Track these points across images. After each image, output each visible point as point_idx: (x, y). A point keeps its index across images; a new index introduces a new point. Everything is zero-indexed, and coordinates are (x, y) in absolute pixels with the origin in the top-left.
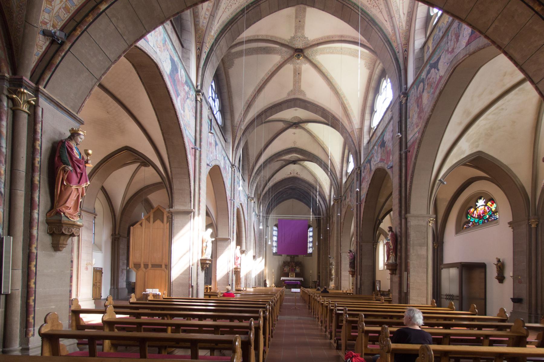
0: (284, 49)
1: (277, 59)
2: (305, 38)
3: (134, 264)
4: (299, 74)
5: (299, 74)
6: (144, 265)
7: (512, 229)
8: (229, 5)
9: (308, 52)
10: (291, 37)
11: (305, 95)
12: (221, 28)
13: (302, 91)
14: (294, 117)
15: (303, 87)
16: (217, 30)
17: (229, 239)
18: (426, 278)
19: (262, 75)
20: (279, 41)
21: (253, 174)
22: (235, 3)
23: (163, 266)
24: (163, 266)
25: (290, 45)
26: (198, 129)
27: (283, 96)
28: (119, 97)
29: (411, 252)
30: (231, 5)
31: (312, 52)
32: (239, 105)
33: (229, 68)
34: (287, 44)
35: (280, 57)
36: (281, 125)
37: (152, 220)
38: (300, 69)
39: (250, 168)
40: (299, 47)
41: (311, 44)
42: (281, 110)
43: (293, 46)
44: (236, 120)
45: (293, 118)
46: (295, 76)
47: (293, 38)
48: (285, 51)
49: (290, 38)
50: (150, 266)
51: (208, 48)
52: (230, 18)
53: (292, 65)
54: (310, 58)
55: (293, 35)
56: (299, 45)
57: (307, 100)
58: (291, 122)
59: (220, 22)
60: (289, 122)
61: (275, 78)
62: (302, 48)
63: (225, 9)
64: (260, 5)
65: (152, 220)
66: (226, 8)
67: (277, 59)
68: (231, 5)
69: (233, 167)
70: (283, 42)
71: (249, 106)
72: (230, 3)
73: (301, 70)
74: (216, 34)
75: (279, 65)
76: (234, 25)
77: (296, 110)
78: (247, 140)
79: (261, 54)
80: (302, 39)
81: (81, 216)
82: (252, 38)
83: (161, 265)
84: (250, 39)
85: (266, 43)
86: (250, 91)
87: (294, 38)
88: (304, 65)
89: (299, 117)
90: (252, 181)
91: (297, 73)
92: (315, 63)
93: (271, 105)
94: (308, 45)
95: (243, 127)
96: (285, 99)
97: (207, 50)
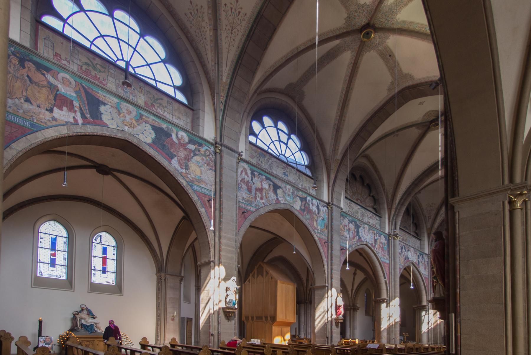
0: (348, 39)
1: (347, 57)
2: (363, 6)
3: (246, 317)
4: (390, 56)
5: (390, 56)
6: (251, 317)
7: (155, 134)
8: (232, 40)
9: (380, 20)
10: (345, 19)
11: (412, 77)
12: (232, 69)
13: (406, 74)
14: (427, 113)
15: (405, 70)
16: (229, 74)
17: (325, 286)
18: (461, 327)
19: (340, 86)
20: (331, 35)
21: (395, 205)
22: (238, 34)
23: (264, 318)
24: (264, 318)
25: (350, 29)
26: (218, 180)
27: (383, 95)
28: (143, 177)
29: (461, 274)
30: (234, 40)
31: (386, 15)
32: (327, 135)
33: (301, 101)
34: (345, 31)
35: (350, 52)
36: (415, 132)
37: (256, 276)
38: (387, 48)
39: (390, 200)
40: (363, 23)
41: (375, 8)
42: (389, 115)
43: (355, 28)
44: (328, 152)
45: (424, 116)
46: (387, 63)
47: (349, 19)
48: (352, 41)
49: (344, 21)
50: (255, 318)
51: (223, 97)
52: (238, 53)
53: (372, 51)
54: (389, 25)
55: (346, 16)
56: (361, 20)
57: (417, 82)
58: (425, 122)
59: (229, 63)
60: (424, 123)
61: (358, 82)
62: (367, 21)
63: (228, 48)
64: (262, 15)
65: (256, 276)
66: (229, 46)
67: (347, 57)
68: (234, 40)
69: (329, 206)
70: (338, 32)
71: (338, 130)
72: (232, 38)
73: (389, 49)
74: (229, 78)
75: (353, 62)
76: (243, 56)
77: (422, 103)
78: (4, 179)
79: (328, 63)
80: (360, 10)
81: (166, 279)
82: (290, 56)
83: (262, 317)
84: (288, 58)
85: (312, 49)
86: (333, 113)
87: (349, 17)
88: (388, 41)
89: (433, 111)
90: (394, 214)
91: (388, 56)
92: (399, 26)
93: (369, 116)
94: (372, 12)
95: (339, 157)
96: (387, 98)
97: (223, 99)
